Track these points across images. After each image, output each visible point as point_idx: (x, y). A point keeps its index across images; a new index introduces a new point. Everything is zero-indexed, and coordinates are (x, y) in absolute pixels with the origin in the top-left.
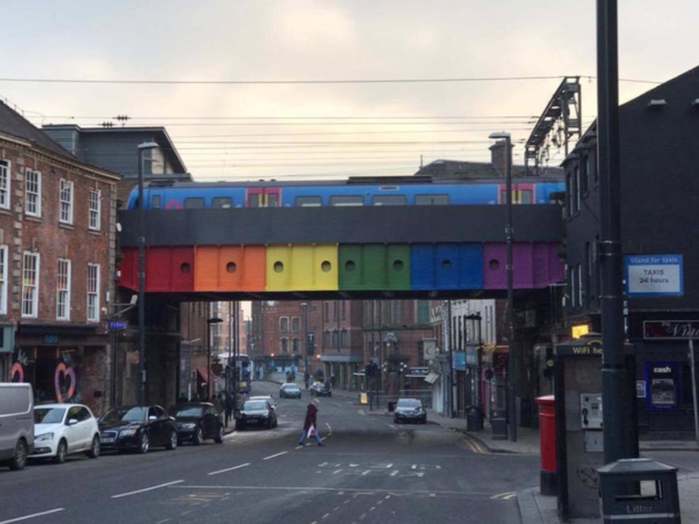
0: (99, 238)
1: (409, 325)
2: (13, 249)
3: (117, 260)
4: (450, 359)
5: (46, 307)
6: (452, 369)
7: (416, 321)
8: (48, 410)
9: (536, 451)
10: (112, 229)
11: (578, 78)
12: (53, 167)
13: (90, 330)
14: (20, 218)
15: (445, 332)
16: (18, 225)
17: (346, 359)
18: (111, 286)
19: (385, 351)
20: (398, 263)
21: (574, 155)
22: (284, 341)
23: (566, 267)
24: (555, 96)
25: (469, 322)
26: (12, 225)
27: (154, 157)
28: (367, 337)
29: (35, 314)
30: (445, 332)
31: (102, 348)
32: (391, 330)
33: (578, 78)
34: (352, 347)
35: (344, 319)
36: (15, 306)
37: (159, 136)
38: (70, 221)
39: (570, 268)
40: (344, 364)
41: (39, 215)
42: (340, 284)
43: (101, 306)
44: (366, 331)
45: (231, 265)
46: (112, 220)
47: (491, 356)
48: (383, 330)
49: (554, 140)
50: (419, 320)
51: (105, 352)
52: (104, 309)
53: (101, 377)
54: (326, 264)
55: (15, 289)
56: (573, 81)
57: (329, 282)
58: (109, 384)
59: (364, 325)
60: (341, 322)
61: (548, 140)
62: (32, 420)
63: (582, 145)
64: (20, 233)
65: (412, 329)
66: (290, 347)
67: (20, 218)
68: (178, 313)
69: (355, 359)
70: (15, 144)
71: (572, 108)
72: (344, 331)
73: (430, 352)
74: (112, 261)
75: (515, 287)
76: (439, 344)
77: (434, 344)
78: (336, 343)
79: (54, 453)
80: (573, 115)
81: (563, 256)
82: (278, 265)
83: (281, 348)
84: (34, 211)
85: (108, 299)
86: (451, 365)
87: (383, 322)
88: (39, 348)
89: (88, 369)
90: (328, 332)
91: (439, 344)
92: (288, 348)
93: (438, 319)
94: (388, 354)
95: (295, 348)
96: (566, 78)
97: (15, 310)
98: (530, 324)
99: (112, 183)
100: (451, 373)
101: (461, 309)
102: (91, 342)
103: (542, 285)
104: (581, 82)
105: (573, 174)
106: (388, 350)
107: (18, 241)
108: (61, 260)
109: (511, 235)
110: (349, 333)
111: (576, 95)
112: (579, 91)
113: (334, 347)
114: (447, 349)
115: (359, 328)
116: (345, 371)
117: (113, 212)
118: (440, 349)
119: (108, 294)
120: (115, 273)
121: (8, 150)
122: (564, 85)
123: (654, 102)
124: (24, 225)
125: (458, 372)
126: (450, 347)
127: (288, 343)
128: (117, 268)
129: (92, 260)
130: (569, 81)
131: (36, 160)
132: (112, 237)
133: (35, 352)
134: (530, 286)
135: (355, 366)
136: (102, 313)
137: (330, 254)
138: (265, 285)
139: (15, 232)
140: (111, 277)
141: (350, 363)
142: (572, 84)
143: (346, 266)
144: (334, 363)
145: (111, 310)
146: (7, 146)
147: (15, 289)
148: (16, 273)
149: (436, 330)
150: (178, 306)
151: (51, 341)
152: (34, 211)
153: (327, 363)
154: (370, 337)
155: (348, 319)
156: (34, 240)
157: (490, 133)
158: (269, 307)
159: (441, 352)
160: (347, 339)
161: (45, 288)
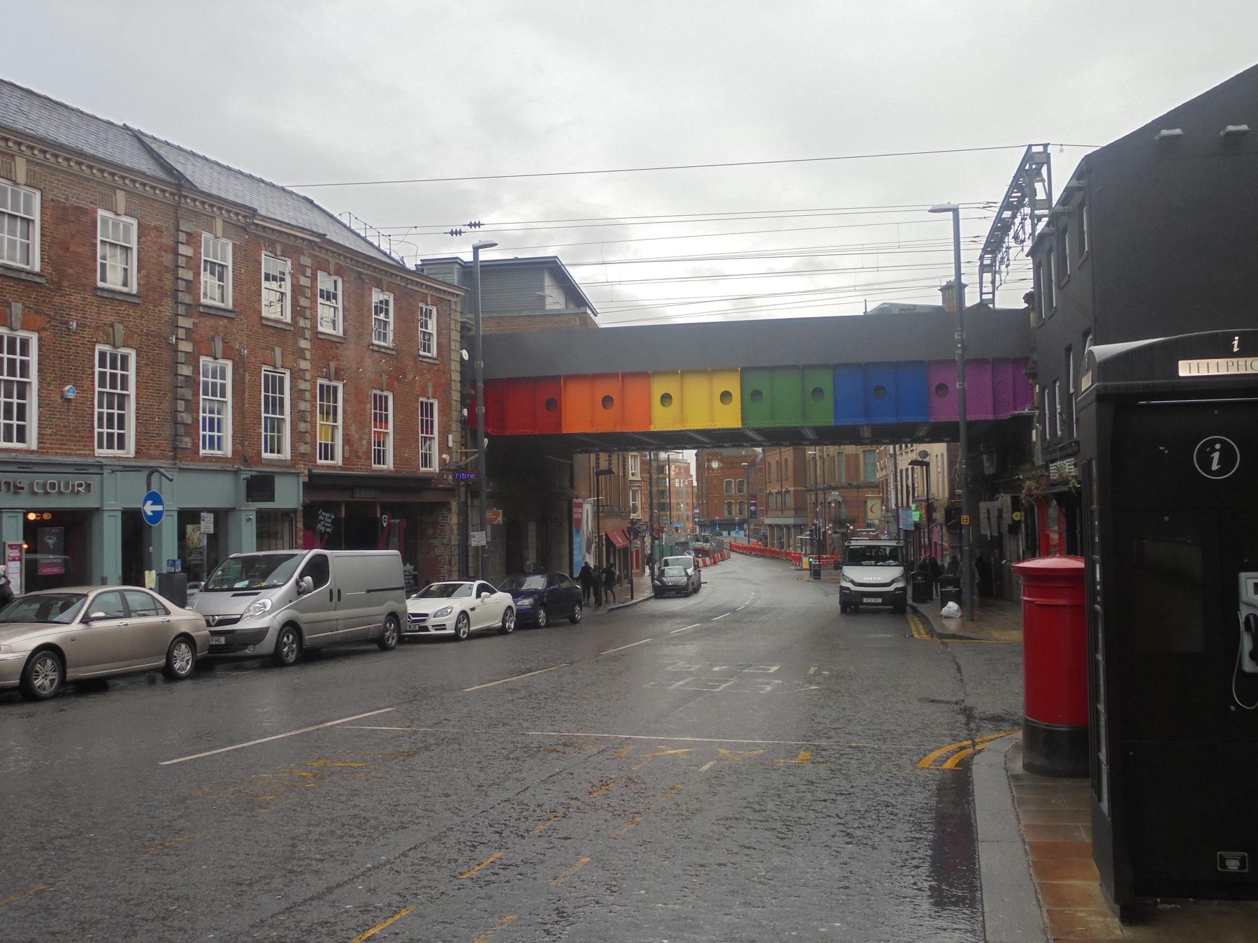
0: (439, 368)
1: (855, 483)
2: (296, 375)
3: (463, 396)
4: (897, 518)
5: (356, 452)
6: (899, 529)
7: (862, 479)
8: (462, 585)
9: (1017, 636)
10: (455, 356)
11: (1046, 146)
12: (360, 273)
13: (424, 483)
14: (308, 334)
15: (892, 486)
16: (304, 344)
17: (790, 521)
18: (455, 426)
19: (830, 513)
20: (818, 392)
21: (1060, 208)
22: (729, 504)
23: (1037, 389)
24: (1016, 178)
25: (918, 468)
26: (296, 343)
27: (547, 292)
28: (811, 498)
29: (339, 460)
30: (892, 486)
31: (446, 505)
32: (835, 489)
33: (1046, 146)
34: (796, 510)
35: (787, 480)
36: (303, 448)
37: (553, 269)
38: (389, 342)
39: (1042, 390)
40: (788, 527)
41: (341, 333)
42: (743, 419)
43: (441, 453)
44: (809, 491)
45: (607, 401)
46: (455, 345)
47: (943, 512)
48: (827, 489)
49: (1016, 238)
50: (866, 477)
51: (449, 509)
52: (444, 456)
53: (445, 541)
54: (726, 396)
55: (303, 426)
56: (1040, 149)
57: (729, 418)
58: (456, 550)
59: (808, 485)
60: (784, 482)
61: (1009, 240)
62: (402, 592)
63: (1075, 183)
64: (308, 355)
65: (858, 487)
66: (735, 509)
67: (308, 334)
68: (571, 467)
69: (799, 521)
70: (296, 237)
71: (1038, 186)
72: (788, 491)
73: (875, 512)
74: (456, 396)
75: (970, 418)
76: (885, 501)
77: (879, 502)
78: (779, 505)
79: (450, 631)
80: (1041, 195)
81: (1034, 376)
82: (666, 398)
83: (726, 512)
84: (332, 459)
85: (450, 444)
86: (898, 525)
87: (826, 481)
88: (348, 504)
89: (430, 532)
90: (771, 493)
91: (885, 501)
92: (733, 512)
93: (884, 473)
94: (833, 515)
95: (741, 512)
96: (1030, 146)
97: (303, 455)
98: (989, 469)
99: (454, 299)
100: (898, 534)
101: (907, 455)
102: (429, 497)
103: (1005, 416)
104: (1050, 150)
105: (1044, 263)
106: (833, 510)
107: (304, 365)
108: (378, 392)
109: (962, 341)
110: (792, 494)
111: (1044, 170)
112: (1048, 163)
113: (777, 510)
114: (894, 507)
115: (803, 488)
116: (902, 550)
117: (455, 336)
118: (887, 507)
119: (450, 437)
120: (461, 411)
121: (285, 246)
122: (1028, 157)
123: (1164, 132)
124: (313, 345)
125: (906, 531)
126: (897, 504)
127: (733, 506)
128: (463, 404)
129: (424, 394)
130: (1034, 149)
131: (332, 262)
132: (455, 366)
133: (343, 509)
134: (991, 417)
135: (800, 528)
136: (442, 462)
137: (732, 384)
138: (650, 422)
139: (300, 353)
140: (455, 415)
141: (795, 526)
142: (1040, 153)
143: (752, 397)
144: (778, 526)
145: (456, 457)
146: (284, 239)
147: (303, 426)
148: (303, 406)
149: (880, 487)
150: (572, 459)
151: (362, 496)
152: (332, 459)
153: (770, 526)
154: (813, 497)
155: (791, 480)
156: (333, 365)
157: (929, 208)
158: (713, 470)
159: (887, 510)
160: (790, 500)
161: (353, 428)
